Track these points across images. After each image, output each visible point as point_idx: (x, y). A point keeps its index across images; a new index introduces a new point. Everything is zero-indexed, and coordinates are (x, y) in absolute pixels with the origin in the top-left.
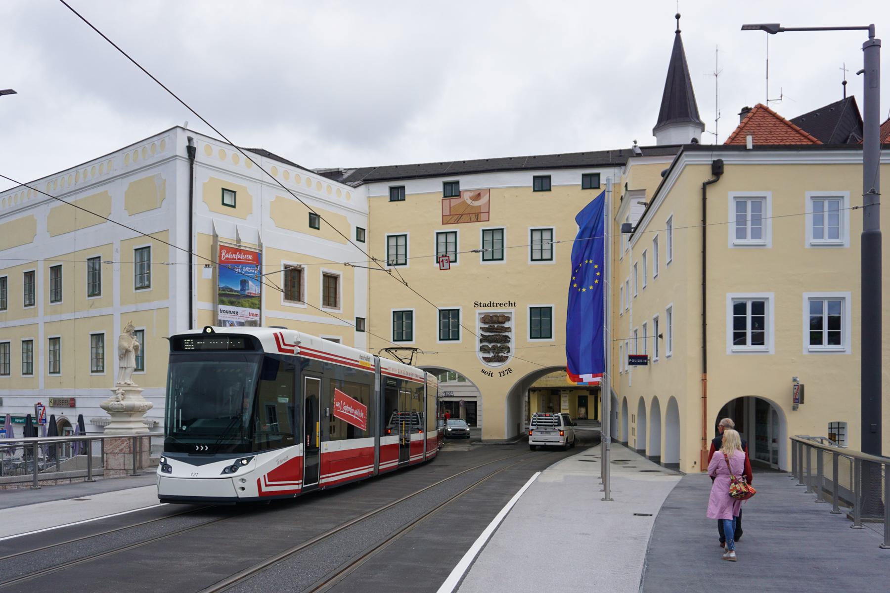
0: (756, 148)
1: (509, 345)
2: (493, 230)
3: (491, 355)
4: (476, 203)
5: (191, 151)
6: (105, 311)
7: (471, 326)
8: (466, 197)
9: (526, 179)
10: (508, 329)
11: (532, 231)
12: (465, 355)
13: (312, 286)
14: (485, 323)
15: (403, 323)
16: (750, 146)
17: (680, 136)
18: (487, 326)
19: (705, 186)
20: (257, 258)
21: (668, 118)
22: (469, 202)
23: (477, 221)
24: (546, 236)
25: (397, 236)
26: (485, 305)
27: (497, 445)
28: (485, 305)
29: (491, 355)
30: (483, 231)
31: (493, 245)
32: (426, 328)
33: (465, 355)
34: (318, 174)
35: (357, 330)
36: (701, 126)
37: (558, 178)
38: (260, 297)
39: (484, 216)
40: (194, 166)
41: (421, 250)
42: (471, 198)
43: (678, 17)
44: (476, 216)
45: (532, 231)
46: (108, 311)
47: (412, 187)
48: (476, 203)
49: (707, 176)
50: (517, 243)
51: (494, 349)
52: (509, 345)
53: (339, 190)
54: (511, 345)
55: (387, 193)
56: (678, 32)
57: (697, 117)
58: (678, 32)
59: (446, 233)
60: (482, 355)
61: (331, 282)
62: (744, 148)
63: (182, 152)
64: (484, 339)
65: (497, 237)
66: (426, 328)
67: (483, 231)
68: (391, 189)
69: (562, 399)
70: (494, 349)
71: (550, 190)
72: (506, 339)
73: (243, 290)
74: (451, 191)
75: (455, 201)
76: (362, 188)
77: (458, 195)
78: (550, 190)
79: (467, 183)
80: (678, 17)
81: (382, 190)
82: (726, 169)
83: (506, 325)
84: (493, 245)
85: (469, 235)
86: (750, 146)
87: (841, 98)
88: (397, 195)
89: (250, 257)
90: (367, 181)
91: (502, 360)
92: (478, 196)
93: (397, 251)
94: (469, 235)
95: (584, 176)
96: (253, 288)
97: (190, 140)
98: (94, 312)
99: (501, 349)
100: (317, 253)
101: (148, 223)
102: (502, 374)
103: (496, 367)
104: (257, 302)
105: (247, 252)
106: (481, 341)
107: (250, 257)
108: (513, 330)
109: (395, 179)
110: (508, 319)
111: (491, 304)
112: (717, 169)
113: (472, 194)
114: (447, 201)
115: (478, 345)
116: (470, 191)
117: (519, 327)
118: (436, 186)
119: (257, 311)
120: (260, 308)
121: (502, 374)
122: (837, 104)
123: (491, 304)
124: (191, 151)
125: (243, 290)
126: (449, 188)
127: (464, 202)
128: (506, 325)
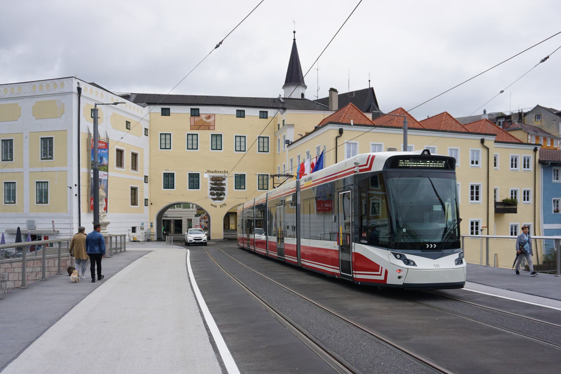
0: (354, 125)
1: (225, 192)
2: (217, 135)
3: (216, 197)
4: (208, 121)
5: (79, 89)
6: (16, 170)
7: (205, 180)
8: (203, 117)
9: (233, 111)
10: (224, 184)
11: (236, 136)
12: (202, 197)
13: (127, 159)
14: (212, 181)
15: (169, 180)
16: (352, 124)
17: (296, 93)
18: (213, 182)
19: (337, 138)
20: (107, 145)
21: (291, 82)
22: (205, 120)
23: (209, 129)
24: (243, 139)
25: (165, 134)
26: (213, 172)
27: (219, 242)
28: (213, 172)
29: (216, 197)
30: (212, 135)
31: (217, 141)
32: (182, 181)
33: (202, 197)
34: (119, 96)
35: (145, 182)
36: (305, 87)
37: (249, 112)
38: (107, 166)
39: (212, 128)
40: (81, 98)
41: (179, 142)
42: (206, 118)
43: (294, 32)
44: (208, 127)
45: (236, 136)
46: (20, 170)
47: (174, 109)
48: (208, 121)
49: (337, 134)
50: (228, 142)
51: (217, 194)
52: (225, 192)
53: (97, 92)
54: (226, 192)
55: (160, 111)
56: (294, 40)
57: (304, 83)
58: (294, 40)
59: (192, 134)
60: (211, 196)
61: (134, 156)
62: (350, 124)
63: (75, 91)
64: (212, 189)
65: (219, 138)
66: (182, 181)
67: (212, 135)
68: (162, 109)
69: (231, 219)
70: (217, 194)
71: (244, 117)
72: (223, 189)
73: (101, 162)
74: (195, 113)
75: (197, 119)
76: (147, 108)
77: (199, 115)
78: (244, 117)
79: (204, 110)
80: (294, 32)
81: (158, 109)
82: (344, 131)
83: (223, 182)
84: (217, 141)
85: (205, 136)
86: (352, 124)
87: (368, 87)
88: (165, 112)
89: (104, 145)
90: (149, 104)
91: (221, 199)
92: (209, 117)
93: (165, 141)
94: (205, 136)
95: (260, 112)
96: (105, 161)
97: (78, 83)
98: (6, 170)
99: (221, 194)
100: (130, 142)
101: (48, 127)
102: (221, 206)
103: (218, 202)
104: (106, 168)
105: (103, 143)
106: (211, 190)
107: (104, 145)
108: (227, 185)
109: (165, 103)
110: (224, 179)
111: (216, 172)
112: (341, 131)
113: (206, 116)
114: (193, 118)
115: (209, 192)
116: (205, 114)
117: (229, 184)
118: (187, 110)
119: (106, 173)
120: (107, 171)
121: (221, 206)
122: (366, 90)
123: (216, 172)
124: (79, 89)
125: (101, 162)
126: (193, 111)
127: (202, 120)
128: (223, 182)
